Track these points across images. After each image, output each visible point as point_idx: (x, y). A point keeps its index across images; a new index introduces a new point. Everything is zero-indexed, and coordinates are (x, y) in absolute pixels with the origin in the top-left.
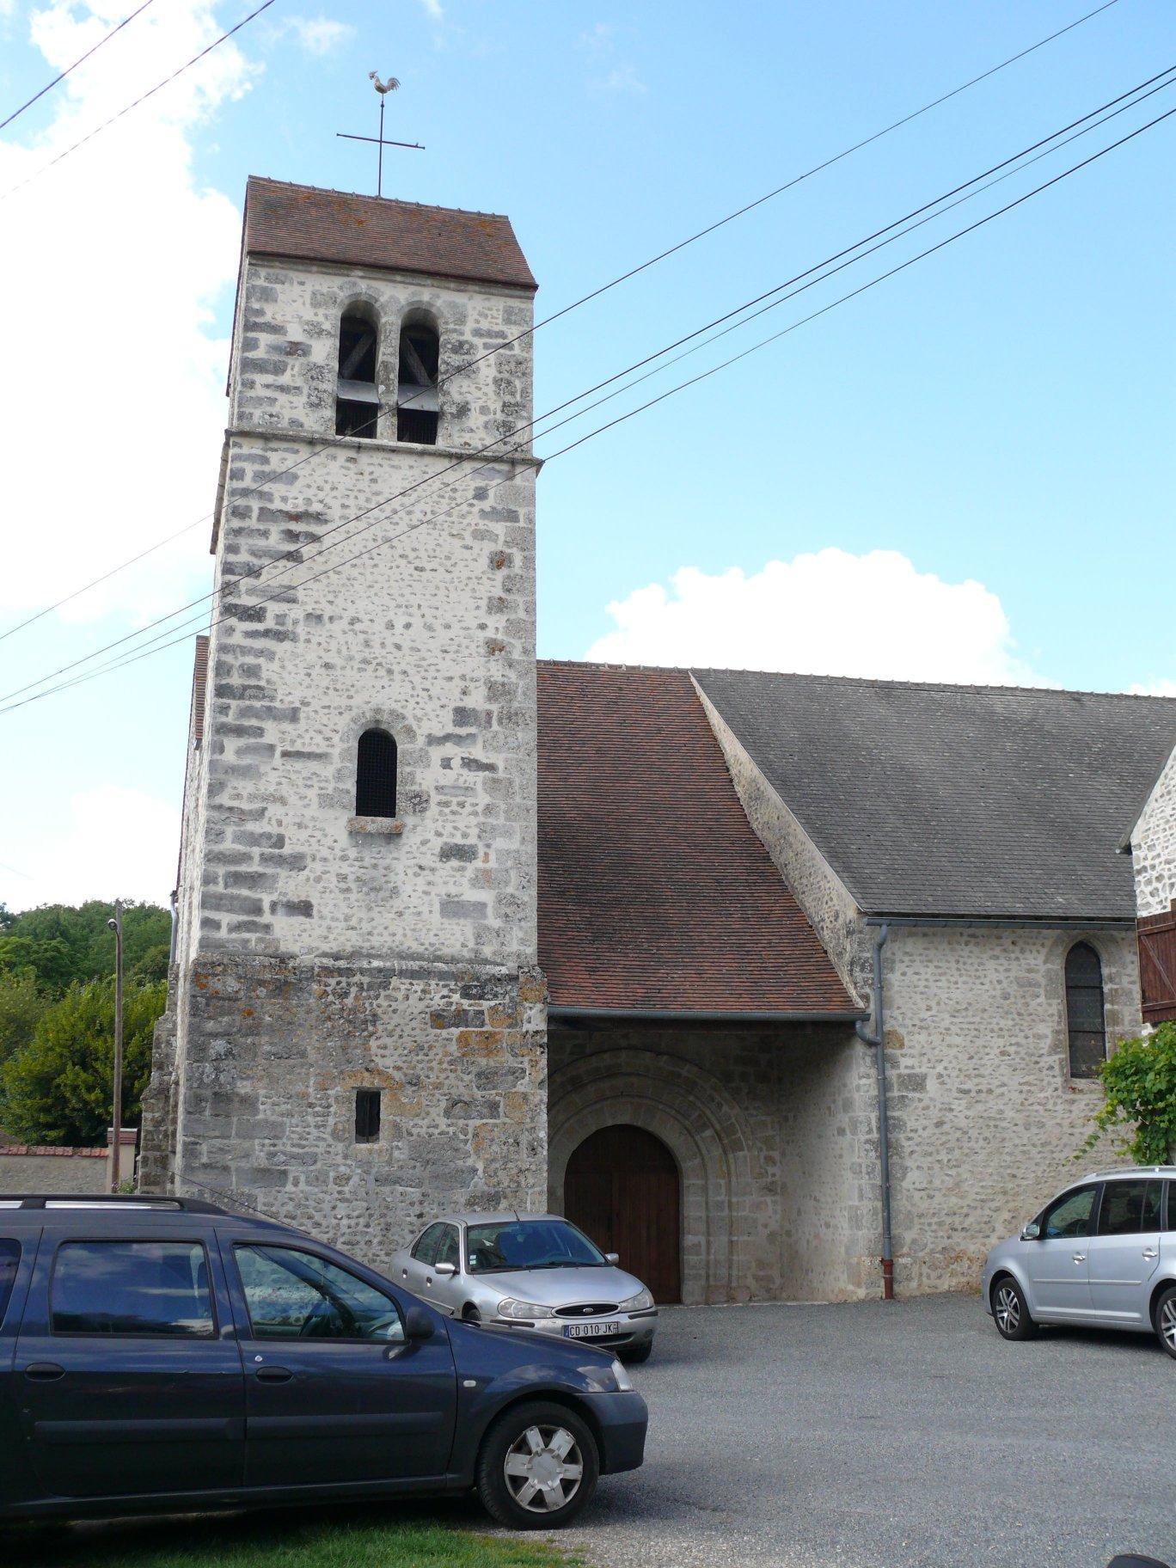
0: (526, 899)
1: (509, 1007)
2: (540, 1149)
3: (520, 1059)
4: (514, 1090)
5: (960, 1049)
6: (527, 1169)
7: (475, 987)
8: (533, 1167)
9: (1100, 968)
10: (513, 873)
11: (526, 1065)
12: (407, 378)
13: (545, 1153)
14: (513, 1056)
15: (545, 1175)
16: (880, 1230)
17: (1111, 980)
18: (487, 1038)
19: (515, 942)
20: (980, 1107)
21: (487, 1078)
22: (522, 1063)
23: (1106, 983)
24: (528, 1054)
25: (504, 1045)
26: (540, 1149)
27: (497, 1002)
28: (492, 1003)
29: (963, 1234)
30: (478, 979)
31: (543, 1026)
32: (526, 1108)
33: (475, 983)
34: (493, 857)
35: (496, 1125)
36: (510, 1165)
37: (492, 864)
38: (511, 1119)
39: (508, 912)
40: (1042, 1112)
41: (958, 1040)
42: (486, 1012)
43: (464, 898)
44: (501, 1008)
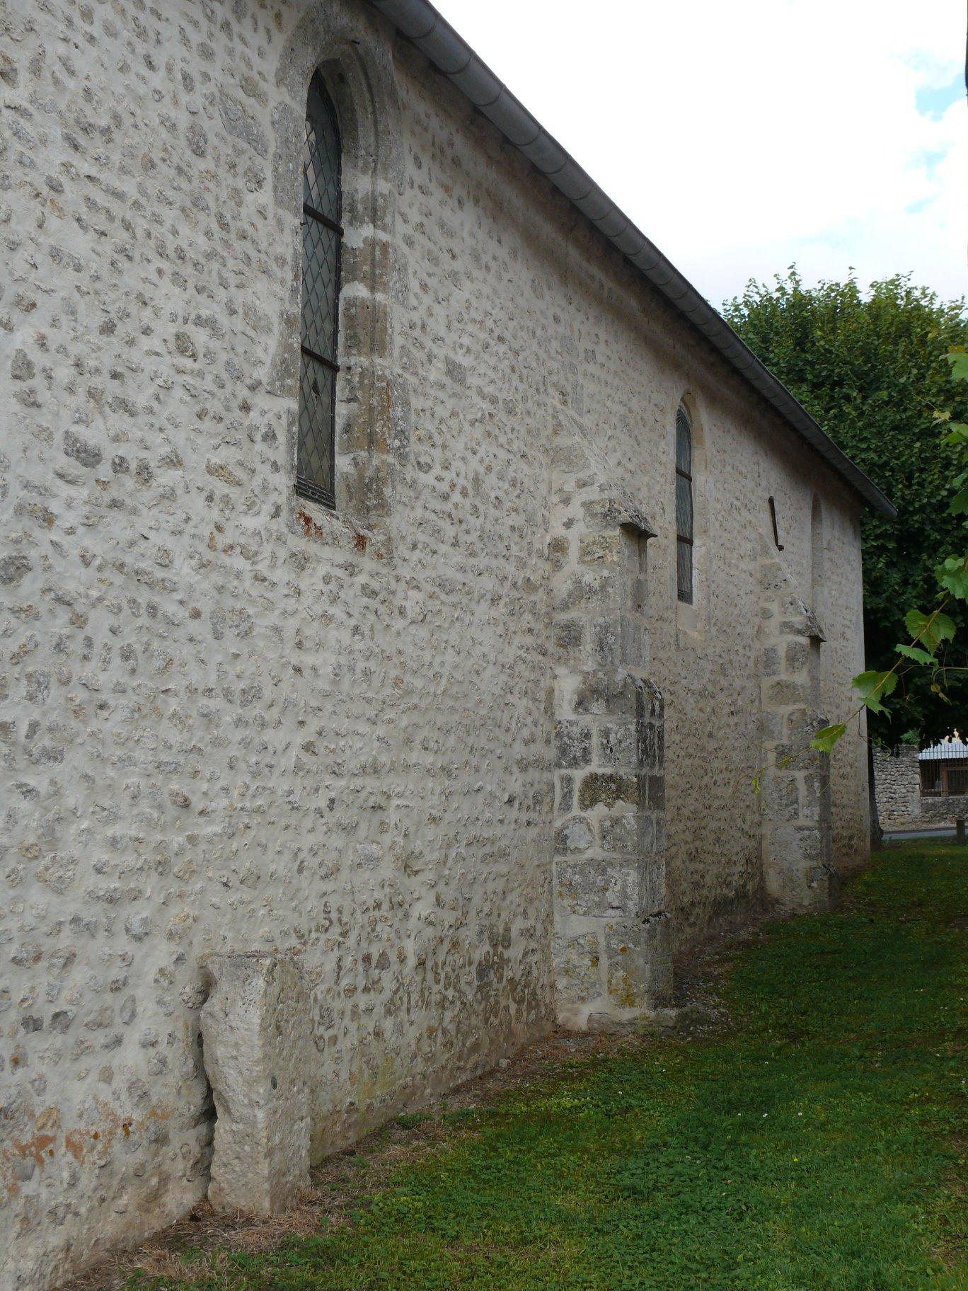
5: (84, 280)
9: (339, 172)
16: (191, 1063)
17: (375, 215)
20: (118, 525)
23: (355, 219)
29: (56, 1040)
40: (248, 577)
41: (79, 244)
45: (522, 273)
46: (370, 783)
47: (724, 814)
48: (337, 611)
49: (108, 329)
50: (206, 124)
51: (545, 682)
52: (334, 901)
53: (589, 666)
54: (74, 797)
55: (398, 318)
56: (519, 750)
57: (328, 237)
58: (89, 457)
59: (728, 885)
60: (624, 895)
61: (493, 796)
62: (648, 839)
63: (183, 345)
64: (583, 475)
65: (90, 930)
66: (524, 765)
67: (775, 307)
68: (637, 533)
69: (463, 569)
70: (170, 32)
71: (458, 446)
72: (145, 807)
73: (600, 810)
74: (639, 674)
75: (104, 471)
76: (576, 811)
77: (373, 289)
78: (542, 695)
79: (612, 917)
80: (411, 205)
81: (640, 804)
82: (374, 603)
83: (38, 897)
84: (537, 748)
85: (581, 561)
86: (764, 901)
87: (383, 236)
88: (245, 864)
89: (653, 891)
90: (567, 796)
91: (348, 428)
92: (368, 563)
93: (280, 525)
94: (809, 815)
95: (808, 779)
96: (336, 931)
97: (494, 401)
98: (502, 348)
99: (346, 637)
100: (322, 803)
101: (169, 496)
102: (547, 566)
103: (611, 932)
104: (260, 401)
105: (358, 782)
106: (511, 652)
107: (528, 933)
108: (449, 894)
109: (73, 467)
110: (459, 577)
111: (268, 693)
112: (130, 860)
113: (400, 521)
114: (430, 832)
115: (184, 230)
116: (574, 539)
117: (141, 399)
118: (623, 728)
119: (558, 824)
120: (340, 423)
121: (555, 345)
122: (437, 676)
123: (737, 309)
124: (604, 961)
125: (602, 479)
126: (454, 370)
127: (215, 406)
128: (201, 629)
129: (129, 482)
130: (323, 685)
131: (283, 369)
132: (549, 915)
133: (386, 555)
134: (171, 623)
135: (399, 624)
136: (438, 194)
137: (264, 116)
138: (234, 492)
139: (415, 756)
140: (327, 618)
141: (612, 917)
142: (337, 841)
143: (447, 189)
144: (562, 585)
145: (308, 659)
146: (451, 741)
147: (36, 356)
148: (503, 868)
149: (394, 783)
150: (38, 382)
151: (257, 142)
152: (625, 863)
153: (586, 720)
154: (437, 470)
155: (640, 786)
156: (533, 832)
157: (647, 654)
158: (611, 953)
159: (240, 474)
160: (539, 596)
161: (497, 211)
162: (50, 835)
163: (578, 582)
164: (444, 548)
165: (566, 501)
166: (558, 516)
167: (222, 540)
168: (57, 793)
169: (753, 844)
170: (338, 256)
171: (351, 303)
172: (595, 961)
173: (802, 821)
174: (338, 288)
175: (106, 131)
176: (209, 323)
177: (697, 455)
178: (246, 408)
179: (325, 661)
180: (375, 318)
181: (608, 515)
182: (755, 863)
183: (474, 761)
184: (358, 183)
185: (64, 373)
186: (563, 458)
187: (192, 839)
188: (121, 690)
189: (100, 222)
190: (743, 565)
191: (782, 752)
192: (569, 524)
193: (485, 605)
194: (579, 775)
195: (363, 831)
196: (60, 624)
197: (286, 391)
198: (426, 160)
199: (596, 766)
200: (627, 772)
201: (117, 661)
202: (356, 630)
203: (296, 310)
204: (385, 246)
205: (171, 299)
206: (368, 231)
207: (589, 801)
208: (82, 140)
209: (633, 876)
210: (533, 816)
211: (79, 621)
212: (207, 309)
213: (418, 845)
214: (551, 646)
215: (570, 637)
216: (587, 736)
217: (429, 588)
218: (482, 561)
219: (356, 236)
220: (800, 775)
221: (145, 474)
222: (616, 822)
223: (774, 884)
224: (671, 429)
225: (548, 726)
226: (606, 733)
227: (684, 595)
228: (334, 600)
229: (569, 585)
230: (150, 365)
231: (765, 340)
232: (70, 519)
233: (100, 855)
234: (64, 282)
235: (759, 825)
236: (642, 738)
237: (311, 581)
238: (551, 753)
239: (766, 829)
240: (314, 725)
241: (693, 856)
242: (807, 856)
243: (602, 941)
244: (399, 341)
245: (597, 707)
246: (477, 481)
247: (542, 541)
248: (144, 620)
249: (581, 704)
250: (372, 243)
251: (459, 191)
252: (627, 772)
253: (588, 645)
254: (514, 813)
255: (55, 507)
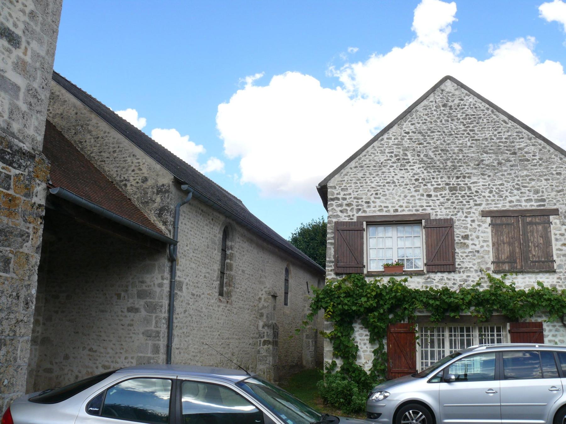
0: (43, 97)
1: (27, 179)
2: (31, 303)
3: (28, 225)
4: (21, 250)
6: (22, 321)
7: (9, 153)
8: (25, 319)
10: (39, 73)
11: (31, 231)
12: (431, 359)
13: (33, 307)
14: (24, 221)
15: (32, 326)
17: (232, 248)
18: (10, 200)
19: (32, 128)
20: (196, 304)
21: (6, 236)
22: (28, 228)
23: (228, 249)
24: (33, 222)
25: (20, 210)
26: (31, 303)
27: (21, 172)
28: (17, 172)
30: (11, 148)
31: (43, 202)
32: (27, 267)
33: (9, 150)
34: (29, 53)
35: (6, 279)
36: (12, 316)
37: (28, 59)
38: (17, 275)
39: (32, 102)
41: (193, 266)
42: (12, 177)
43: (6, 75)
44: (22, 178)
45: (255, 251)
46: (228, 341)
47: (294, 348)
48: (224, 314)
49: (196, 277)
50: (209, 243)
51: (257, 323)
52: (222, 359)
53: (265, 320)
54: (190, 342)
55: (234, 265)
56: (252, 335)
57: (224, 253)
58: (193, 295)
59: (294, 362)
60: (270, 362)
61: (247, 343)
62: (274, 352)
63: (205, 277)
64: (265, 286)
65: (191, 360)
66: (252, 338)
67: (319, 225)
68: (274, 297)
69: (243, 305)
70: (205, 232)
71: (243, 284)
72: (198, 343)
73: (266, 346)
74: (274, 322)
75: (195, 297)
76: (262, 346)
77: (231, 261)
78: (256, 325)
79: (267, 365)
80: (237, 246)
81: (273, 345)
82: (229, 312)
83: (186, 355)
84: (255, 335)
85: (264, 301)
86: (302, 366)
87: (233, 252)
88: (210, 353)
89: (275, 361)
90: (260, 344)
91: (226, 283)
92: (229, 305)
93: (216, 301)
94: (312, 349)
95: (312, 341)
96: (222, 364)
97: (249, 275)
98: (251, 265)
99: (225, 317)
100: (221, 344)
101: (203, 299)
102: (258, 302)
103: (267, 368)
104: (215, 283)
105: (226, 341)
106: (251, 318)
107: (252, 368)
108: (239, 360)
109: (192, 297)
110: (243, 306)
111: (214, 327)
112: (196, 351)
113: (233, 298)
114: (236, 349)
115: (206, 260)
116: (263, 297)
117: (200, 286)
118: (270, 332)
119: (258, 349)
120: (225, 282)
121: (261, 262)
122: (238, 323)
123: (309, 225)
124: (266, 373)
125: (268, 287)
126: (243, 271)
127: (209, 285)
128: (206, 318)
129: (198, 298)
130: (222, 325)
131: (218, 277)
132: (256, 365)
133: (231, 304)
134: (202, 317)
135: (233, 315)
136: (241, 242)
137: (216, 239)
138: (210, 297)
139: (234, 336)
140: (222, 315)
141: (267, 365)
142: (222, 350)
143: (243, 241)
144: (260, 306)
145: (220, 321)
146: (240, 334)
147: (189, 283)
148: (248, 356)
149: (231, 341)
150: (189, 286)
151: (215, 244)
152: (270, 356)
153: (264, 330)
154: (240, 289)
155: (273, 342)
156: (254, 350)
157: (276, 318)
158: (267, 372)
159: (211, 294)
160: (256, 308)
161: (251, 241)
162: (188, 347)
163: (263, 305)
164: (240, 301)
165: (262, 290)
166: (260, 293)
167: (209, 304)
168: (189, 341)
169: (300, 354)
170: (225, 255)
171: (227, 263)
172: (264, 373)
173: (311, 350)
174: (225, 260)
175: (197, 249)
176: (208, 273)
177: (290, 276)
178: (212, 284)
179: (222, 321)
180: (231, 265)
181: (269, 294)
182: (300, 358)
183: (244, 337)
184: (229, 243)
185: (191, 284)
186: (261, 283)
187: (204, 348)
188: (196, 327)
189: (196, 262)
190: (300, 297)
191: (307, 335)
192: (262, 295)
193: (247, 310)
194: (262, 340)
195: (226, 348)
196: (190, 319)
197: (218, 280)
198: (240, 237)
199: (266, 338)
200: (271, 340)
201: (196, 323)
202: (226, 316)
203: (220, 268)
204: (233, 254)
205: (204, 270)
206: (230, 251)
207: (264, 345)
208: (195, 251)
209: (271, 358)
210: (254, 347)
211: (192, 318)
212: (208, 271)
213: (235, 351)
214: (258, 317)
215: (262, 315)
216: (264, 333)
217: (237, 308)
218: (246, 303)
219: (228, 252)
220: (310, 340)
221: (200, 296)
222: (269, 348)
223: (304, 363)
224: (284, 272)
225: (257, 331)
226: (267, 333)
227: (286, 304)
228: (223, 312)
229: (262, 305)
230: (201, 280)
231: (315, 234)
232: (191, 304)
233: (193, 350)
234: (192, 271)
235: (302, 351)
236: (274, 333)
237: (220, 309)
238: (258, 336)
239: (303, 352)
240: (220, 331)
241: (286, 356)
242: (311, 357)
243: (265, 370)
244: (234, 268)
245: (266, 328)
246: (246, 289)
247: (257, 298)
248: (199, 317)
249: (263, 327)
250: (231, 253)
251: (245, 240)
252: (271, 340)
253: (265, 317)
254: (250, 346)
255: (190, 302)
